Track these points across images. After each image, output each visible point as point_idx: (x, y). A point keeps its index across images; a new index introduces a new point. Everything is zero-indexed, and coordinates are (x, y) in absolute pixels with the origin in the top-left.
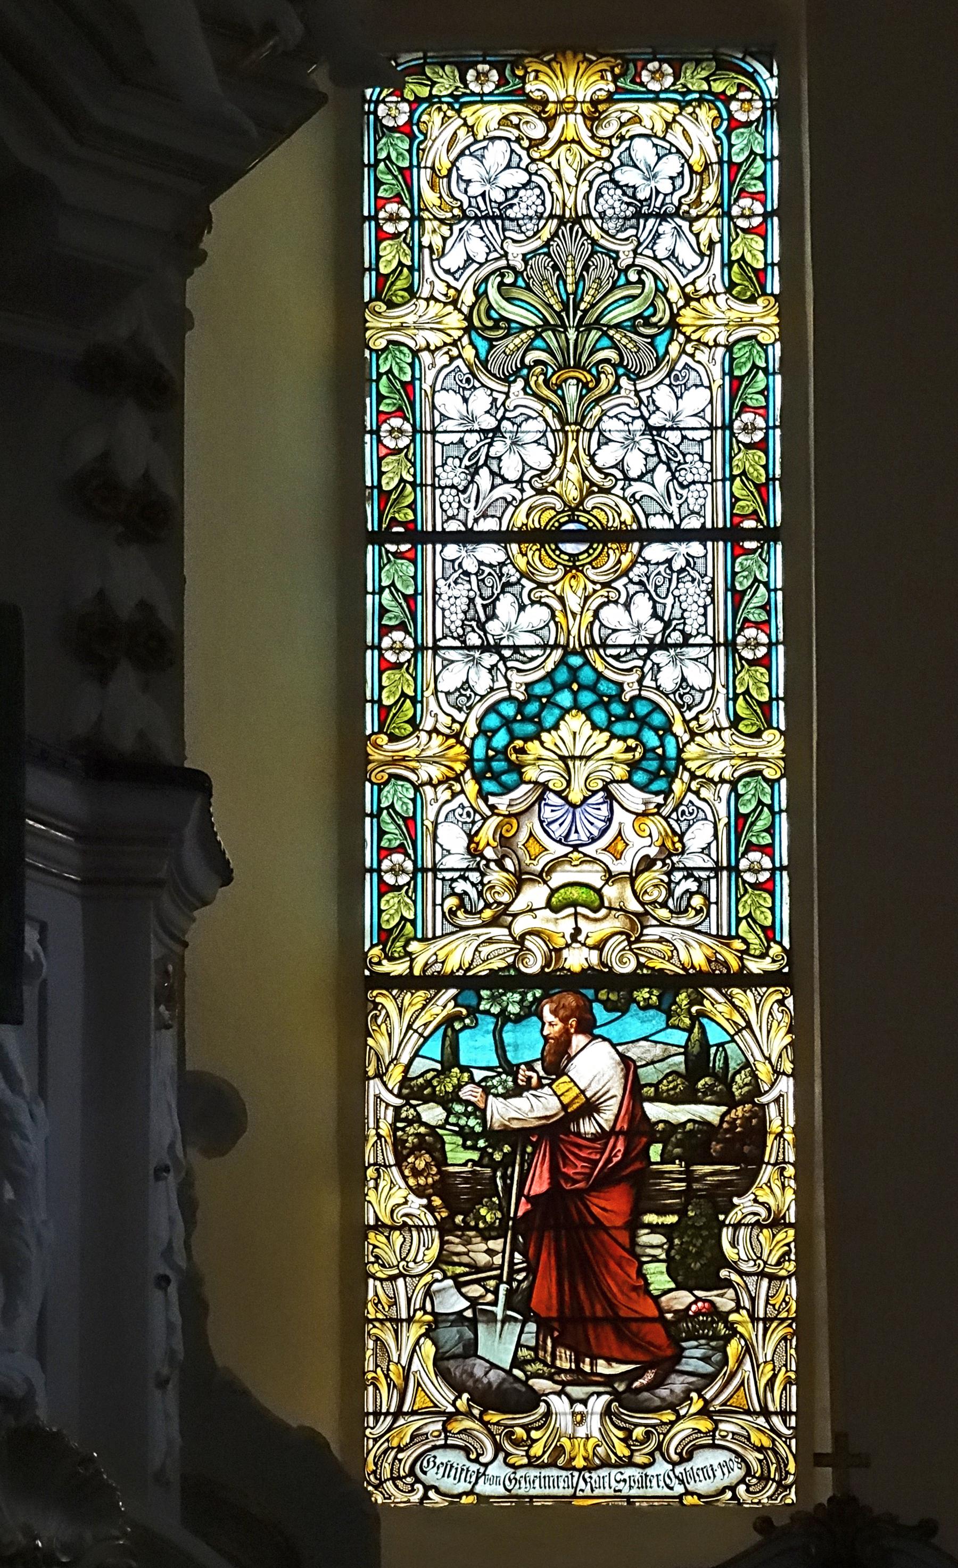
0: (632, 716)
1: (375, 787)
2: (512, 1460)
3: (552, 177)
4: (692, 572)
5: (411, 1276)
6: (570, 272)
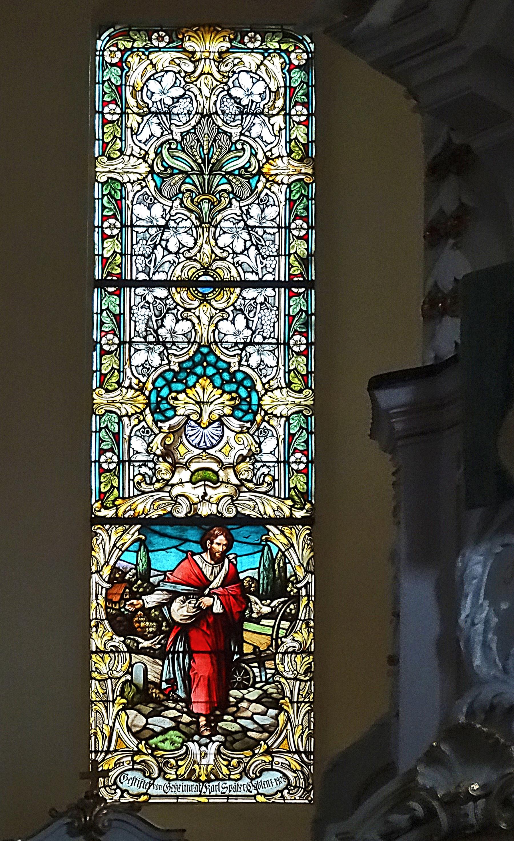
0: (234, 380)
1: (98, 417)
2: (167, 776)
3: (197, 92)
4: (268, 305)
6: (206, 143)
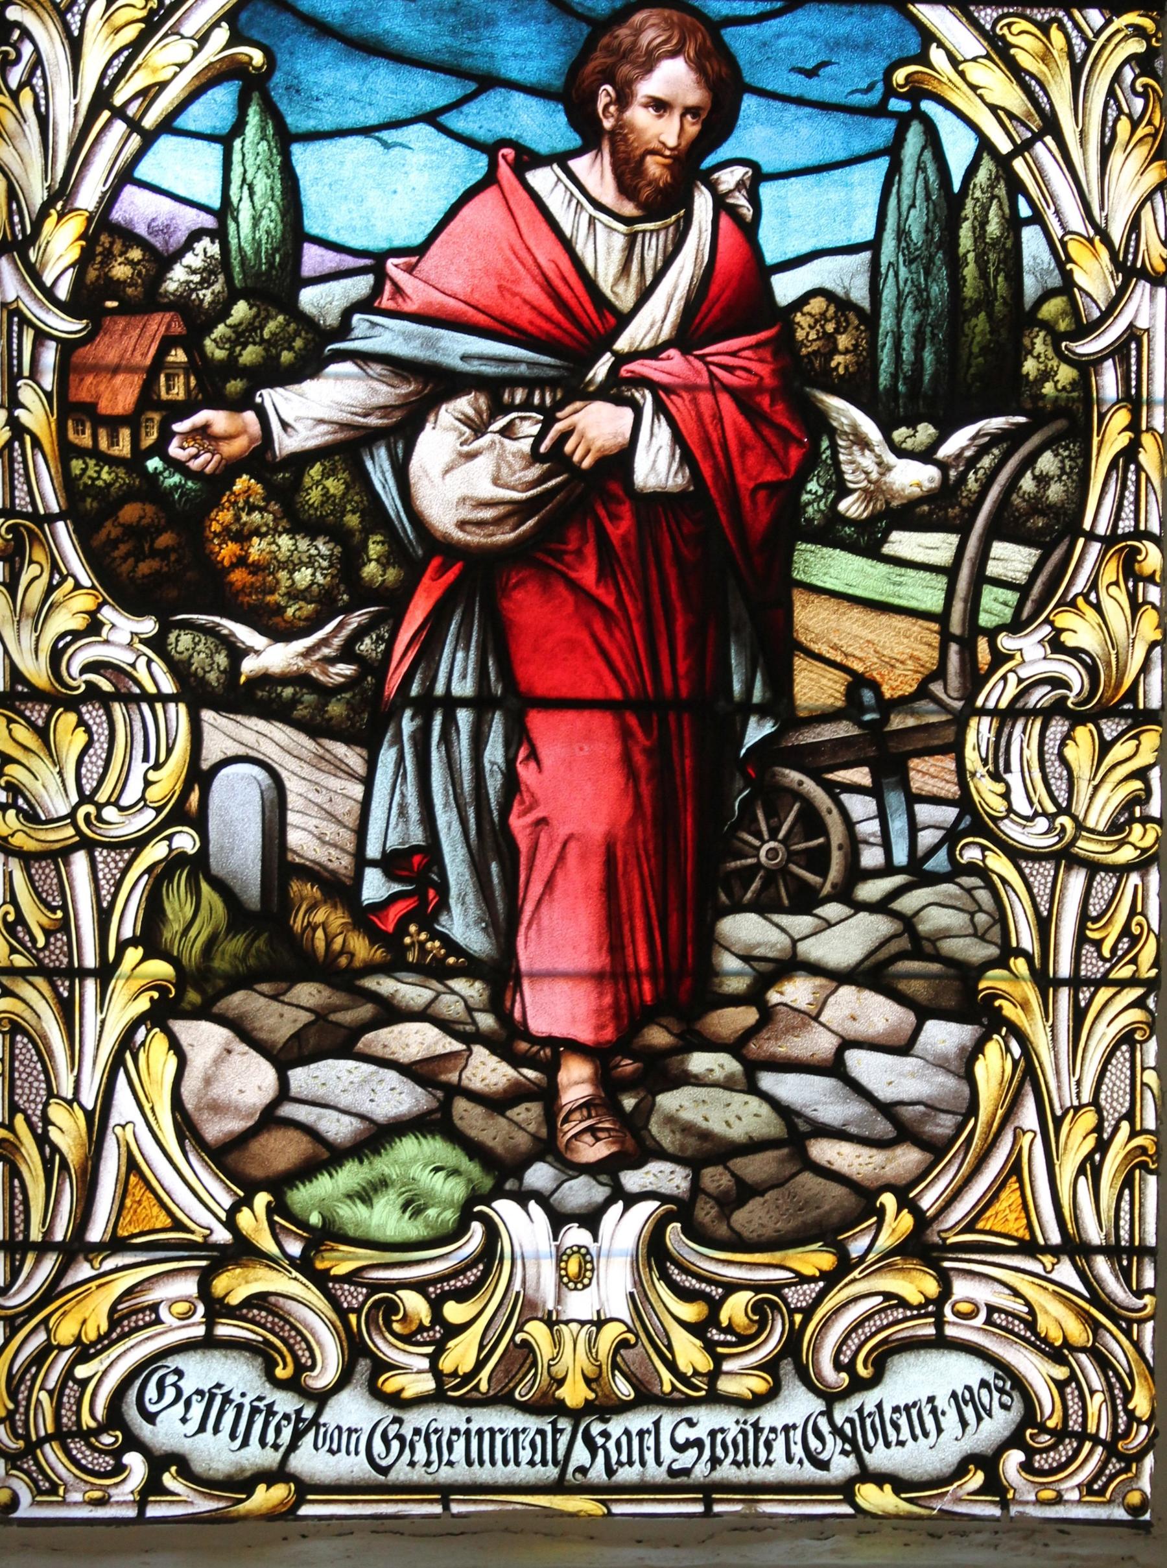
2: (391, 1383)
5: (111, 846)
